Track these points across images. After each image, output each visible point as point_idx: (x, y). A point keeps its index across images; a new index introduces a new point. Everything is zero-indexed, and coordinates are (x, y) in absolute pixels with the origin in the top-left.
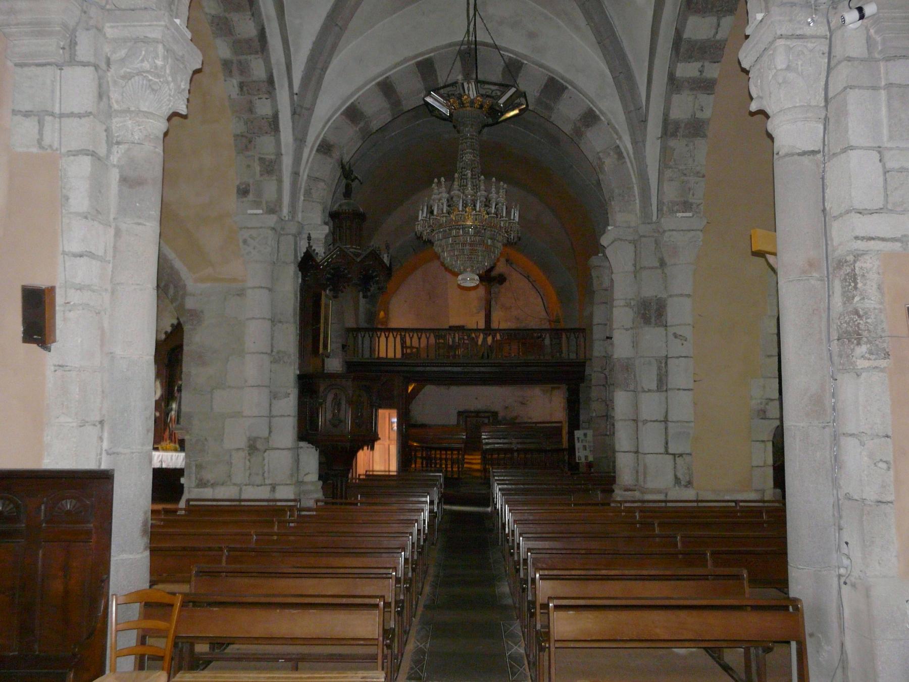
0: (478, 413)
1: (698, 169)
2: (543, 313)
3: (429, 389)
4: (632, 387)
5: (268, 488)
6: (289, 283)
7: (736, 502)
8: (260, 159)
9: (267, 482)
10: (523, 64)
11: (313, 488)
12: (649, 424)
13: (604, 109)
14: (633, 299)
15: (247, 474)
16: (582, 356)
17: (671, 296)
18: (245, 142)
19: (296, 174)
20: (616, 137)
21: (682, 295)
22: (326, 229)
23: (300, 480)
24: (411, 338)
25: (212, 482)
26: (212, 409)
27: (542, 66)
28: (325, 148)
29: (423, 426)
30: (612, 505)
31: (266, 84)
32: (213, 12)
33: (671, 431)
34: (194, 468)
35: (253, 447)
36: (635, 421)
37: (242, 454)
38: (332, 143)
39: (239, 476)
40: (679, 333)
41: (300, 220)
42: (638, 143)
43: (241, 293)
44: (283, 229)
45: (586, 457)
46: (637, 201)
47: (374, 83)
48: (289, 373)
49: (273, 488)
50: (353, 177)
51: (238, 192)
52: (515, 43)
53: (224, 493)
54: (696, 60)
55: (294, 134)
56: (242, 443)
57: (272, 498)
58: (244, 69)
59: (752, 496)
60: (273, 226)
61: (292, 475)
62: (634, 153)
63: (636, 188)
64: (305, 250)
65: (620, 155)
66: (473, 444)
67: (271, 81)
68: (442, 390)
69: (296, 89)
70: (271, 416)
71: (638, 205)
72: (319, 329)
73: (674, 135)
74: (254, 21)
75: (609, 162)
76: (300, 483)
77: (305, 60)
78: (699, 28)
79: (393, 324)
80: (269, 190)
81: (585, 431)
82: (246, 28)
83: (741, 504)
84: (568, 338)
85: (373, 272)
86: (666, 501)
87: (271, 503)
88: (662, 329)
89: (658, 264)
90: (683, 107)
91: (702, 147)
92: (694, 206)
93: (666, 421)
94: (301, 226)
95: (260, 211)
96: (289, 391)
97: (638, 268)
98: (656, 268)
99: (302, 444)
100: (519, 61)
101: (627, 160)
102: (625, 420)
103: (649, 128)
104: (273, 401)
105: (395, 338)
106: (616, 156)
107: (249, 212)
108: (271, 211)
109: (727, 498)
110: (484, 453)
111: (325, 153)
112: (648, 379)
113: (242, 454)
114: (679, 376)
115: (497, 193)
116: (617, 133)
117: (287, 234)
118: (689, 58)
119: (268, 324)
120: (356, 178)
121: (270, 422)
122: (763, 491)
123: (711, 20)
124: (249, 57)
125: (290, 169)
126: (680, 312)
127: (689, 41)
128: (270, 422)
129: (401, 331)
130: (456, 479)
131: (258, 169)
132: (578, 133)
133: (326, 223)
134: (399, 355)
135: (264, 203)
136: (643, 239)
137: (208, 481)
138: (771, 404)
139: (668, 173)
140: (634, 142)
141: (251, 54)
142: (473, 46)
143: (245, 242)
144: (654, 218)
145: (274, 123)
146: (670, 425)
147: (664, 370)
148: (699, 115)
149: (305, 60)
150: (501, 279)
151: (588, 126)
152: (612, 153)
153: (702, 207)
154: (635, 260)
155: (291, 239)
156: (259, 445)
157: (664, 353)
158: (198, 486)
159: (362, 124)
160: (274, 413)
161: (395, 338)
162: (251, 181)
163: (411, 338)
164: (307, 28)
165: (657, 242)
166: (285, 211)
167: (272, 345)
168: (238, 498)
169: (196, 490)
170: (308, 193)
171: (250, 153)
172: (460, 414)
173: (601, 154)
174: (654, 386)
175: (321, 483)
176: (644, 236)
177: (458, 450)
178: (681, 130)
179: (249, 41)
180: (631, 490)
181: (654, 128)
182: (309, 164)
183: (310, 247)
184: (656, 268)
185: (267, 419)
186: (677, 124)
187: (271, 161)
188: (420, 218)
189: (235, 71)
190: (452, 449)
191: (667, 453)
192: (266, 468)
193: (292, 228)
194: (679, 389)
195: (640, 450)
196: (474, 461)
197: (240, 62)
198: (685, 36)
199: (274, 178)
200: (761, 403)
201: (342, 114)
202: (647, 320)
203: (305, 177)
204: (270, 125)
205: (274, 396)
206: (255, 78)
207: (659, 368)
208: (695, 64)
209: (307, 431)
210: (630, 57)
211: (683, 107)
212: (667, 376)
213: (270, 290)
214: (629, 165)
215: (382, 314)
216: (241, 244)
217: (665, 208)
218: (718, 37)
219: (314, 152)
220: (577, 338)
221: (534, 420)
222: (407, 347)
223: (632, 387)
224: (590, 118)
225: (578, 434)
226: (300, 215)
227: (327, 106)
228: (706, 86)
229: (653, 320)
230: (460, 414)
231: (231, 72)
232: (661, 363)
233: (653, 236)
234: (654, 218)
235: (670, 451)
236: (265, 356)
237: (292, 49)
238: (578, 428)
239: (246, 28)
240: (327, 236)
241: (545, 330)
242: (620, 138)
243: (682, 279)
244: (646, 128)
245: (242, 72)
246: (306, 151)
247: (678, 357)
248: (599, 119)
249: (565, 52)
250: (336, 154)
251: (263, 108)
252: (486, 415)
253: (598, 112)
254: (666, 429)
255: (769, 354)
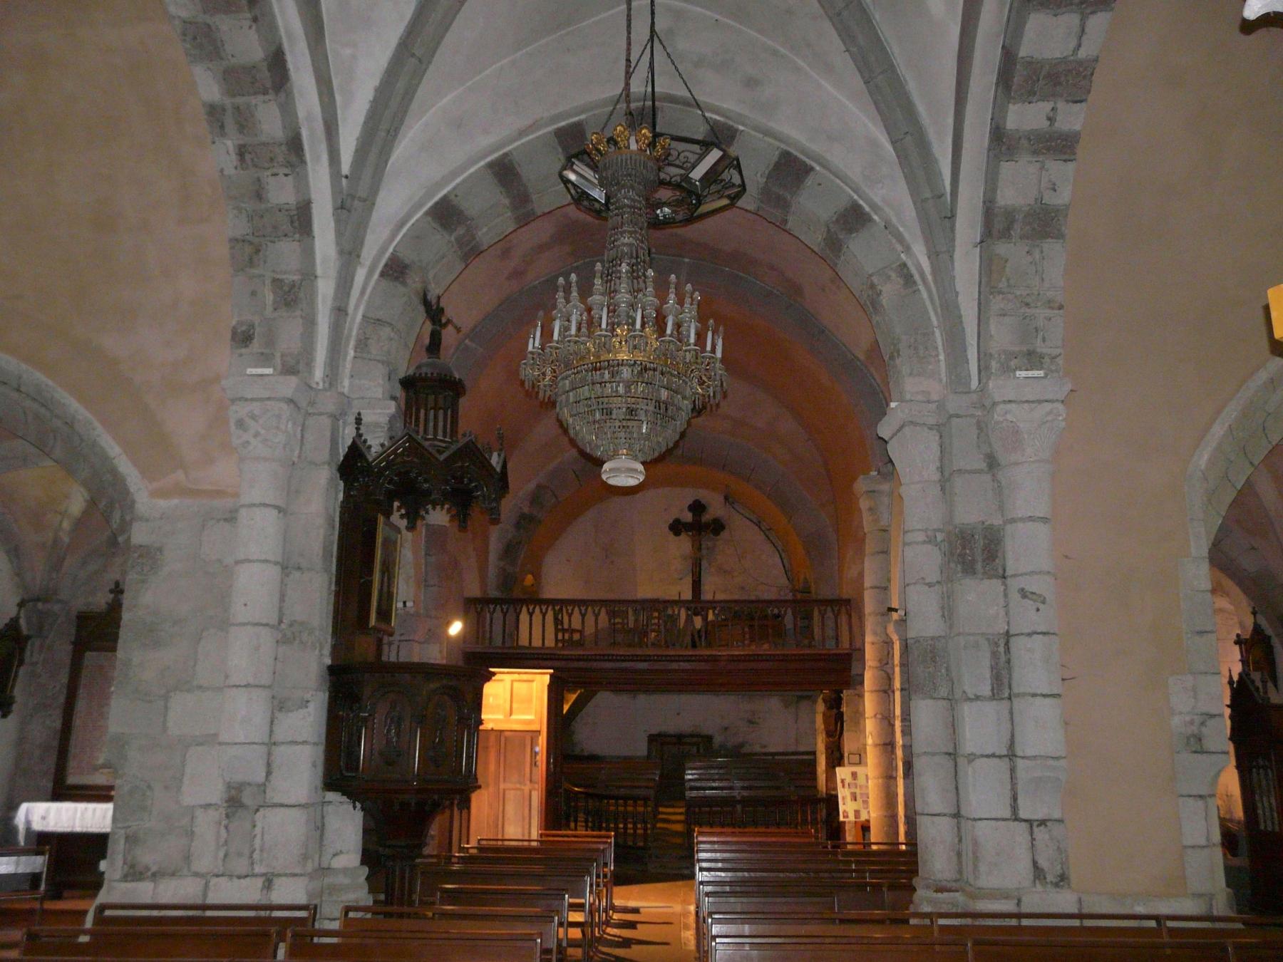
0: (679, 738)
1: (1050, 294)
2: (783, 581)
3: (604, 699)
4: (943, 692)
5: (259, 882)
6: (321, 500)
7: (1157, 918)
8: (274, 281)
9: (257, 870)
10: (737, 130)
11: (346, 881)
12: (978, 762)
13: (877, 200)
14: (939, 530)
15: (221, 854)
16: (845, 644)
17: (1013, 521)
18: (249, 252)
19: (340, 311)
20: (899, 248)
21: (1031, 519)
22: (392, 408)
23: (325, 865)
24: (570, 616)
25: (154, 869)
26: (165, 728)
27: (768, 133)
28: (395, 270)
29: (593, 758)
30: (912, 921)
31: (283, 148)
32: (184, 14)
33: (1021, 774)
34: (122, 842)
35: (234, 802)
36: (953, 755)
37: (214, 815)
38: (407, 261)
39: (204, 863)
40: (1028, 588)
41: (346, 391)
42: (941, 254)
43: (231, 518)
44: (312, 403)
45: (857, 813)
46: (942, 357)
47: (482, 163)
48: (312, 661)
49: (268, 884)
50: (444, 320)
51: (233, 339)
52: (722, 97)
53: (176, 891)
54: (1044, 99)
55: (338, 244)
56: (215, 793)
57: (264, 902)
58: (245, 121)
59: (1188, 906)
60: (289, 396)
61: (305, 857)
62: (934, 273)
63: (937, 333)
64: (349, 442)
65: (908, 279)
66: (671, 787)
67: (295, 145)
68: (624, 699)
69: (346, 168)
70: (271, 744)
71: (943, 364)
72: (369, 584)
73: (1006, 234)
74: (258, 31)
75: (889, 291)
76: (324, 870)
77: (361, 119)
78: (1047, 37)
79: (550, 592)
80: (289, 334)
81: (854, 769)
82: (245, 45)
83: (1170, 924)
84: (823, 616)
85: (470, 481)
86: (1019, 916)
87: (262, 913)
88: (996, 584)
89: (984, 465)
90: (1020, 184)
91: (1055, 256)
92: (1047, 360)
93: (1011, 755)
94: (346, 401)
95: (269, 371)
96: (308, 696)
97: (947, 474)
98: (979, 472)
99: (331, 796)
100: (730, 128)
101: (921, 287)
102: (934, 754)
103: (958, 225)
104: (277, 714)
105: (544, 616)
106: (901, 281)
107: (250, 371)
108: (289, 370)
109: (1140, 910)
110: (692, 805)
111: (397, 279)
112: (974, 674)
113: (214, 815)
114: (1033, 669)
115: (681, 302)
116: (901, 239)
117: (321, 414)
118: (1030, 95)
119: (275, 571)
120: (449, 321)
121: (269, 754)
122: (1211, 897)
123: (1070, 20)
124: (253, 100)
125: (329, 303)
126: (1029, 550)
127: (1030, 63)
128: (269, 754)
129: (560, 604)
130: (643, 848)
131: (270, 298)
132: (834, 245)
133: (393, 398)
134: (550, 642)
135: (278, 355)
136: (955, 421)
137: (148, 869)
138: (1211, 723)
139: (997, 303)
140: (933, 254)
141: (255, 93)
142: (649, 103)
143: (240, 424)
144: (974, 384)
145: (302, 219)
146: (1020, 763)
147: (1003, 659)
148: (1049, 198)
149: (362, 119)
150: (717, 527)
151: (850, 231)
152: (893, 275)
153: (1060, 361)
154: (941, 460)
155: (326, 422)
156: (247, 798)
157: (1002, 628)
158: (125, 878)
159: (461, 231)
160: (278, 736)
161: (544, 616)
162: (256, 320)
163: (570, 616)
164: (365, 65)
165: (981, 427)
166: (319, 373)
167: (281, 609)
168: (199, 901)
169: (124, 885)
170: (362, 345)
171: (255, 271)
172: (652, 739)
173: (875, 280)
174: (986, 691)
175: (366, 870)
176: (958, 416)
177: (646, 799)
178: (1017, 227)
179: (251, 69)
180: (950, 890)
181: (967, 227)
182: (366, 297)
183: (360, 436)
184: (979, 472)
185: (264, 749)
186: (1010, 215)
187: (293, 285)
188: (530, 348)
189: (229, 121)
190: (635, 799)
191: (1016, 818)
192: (258, 842)
193: (328, 404)
194: (1034, 695)
195: (963, 812)
196: (674, 816)
197: (237, 108)
198: (1023, 53)
199: (298, 313)
200: (1192, 722)
201: (427, 213)
202: (969, 569)
203: (359, 317)
204: (292, 222)
205: (280, 705)
206: (263, 139)
207: (994, 654)
208: (1041, 104)
209: (339, 774)
210: (921, 109)
211: (1020, 184)
212: (1010, 669)
213: (280, 509)
214: (925, 295)
215: (529, 579)
216: (233, 427)
217: (994, 364)
218: (1082, 54)
219: (376, 276)
220: (836, 616)
221: (772, 750)
222: (564, 631)
223: (943, 692)
224: (854, 218)
225: (842, 773)
226: (346, 383)
227: (399, 203)
228: (1059, 145)
229: (979, 566)
230: (652, 739)
231: (222, 127)
232: (997, 644)
233: (972, 416)
234: (974, 384)
235: (1022, 815)
236: (265, 632)
237: (338, 98)
238: (840, 764)
239: (245, 45)
240: (392, 419)
241: (786, 601)
242: (908, 249)
243: (1030, 491)
244: (953, 229)
245: (242, 128)
246: (360, 275)
247: (1029, 635)
248: (870, 220)
249: (811, 109)
250: (414, 282)
251: (281, 192)
252: (695, 740)
253: (867, 209)
254: (1013, 770)
255: (1198, 629)
